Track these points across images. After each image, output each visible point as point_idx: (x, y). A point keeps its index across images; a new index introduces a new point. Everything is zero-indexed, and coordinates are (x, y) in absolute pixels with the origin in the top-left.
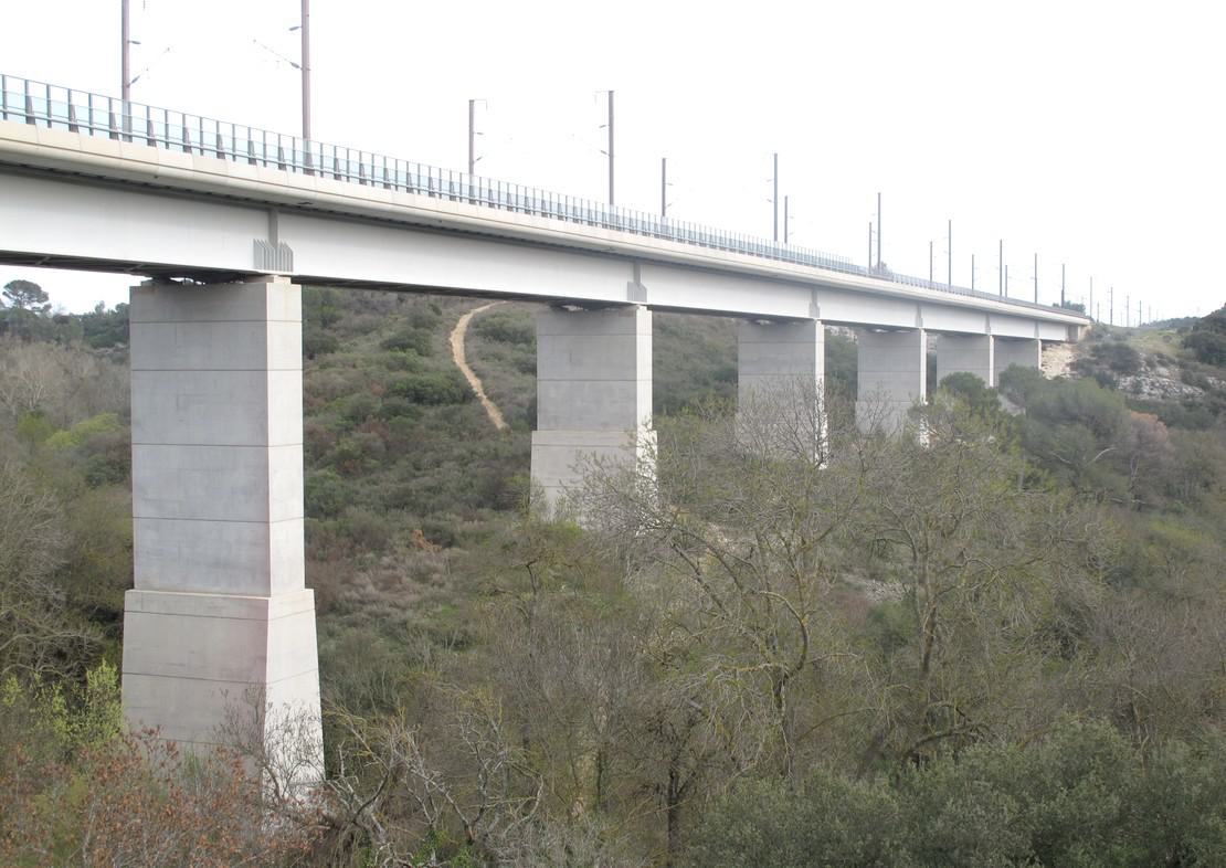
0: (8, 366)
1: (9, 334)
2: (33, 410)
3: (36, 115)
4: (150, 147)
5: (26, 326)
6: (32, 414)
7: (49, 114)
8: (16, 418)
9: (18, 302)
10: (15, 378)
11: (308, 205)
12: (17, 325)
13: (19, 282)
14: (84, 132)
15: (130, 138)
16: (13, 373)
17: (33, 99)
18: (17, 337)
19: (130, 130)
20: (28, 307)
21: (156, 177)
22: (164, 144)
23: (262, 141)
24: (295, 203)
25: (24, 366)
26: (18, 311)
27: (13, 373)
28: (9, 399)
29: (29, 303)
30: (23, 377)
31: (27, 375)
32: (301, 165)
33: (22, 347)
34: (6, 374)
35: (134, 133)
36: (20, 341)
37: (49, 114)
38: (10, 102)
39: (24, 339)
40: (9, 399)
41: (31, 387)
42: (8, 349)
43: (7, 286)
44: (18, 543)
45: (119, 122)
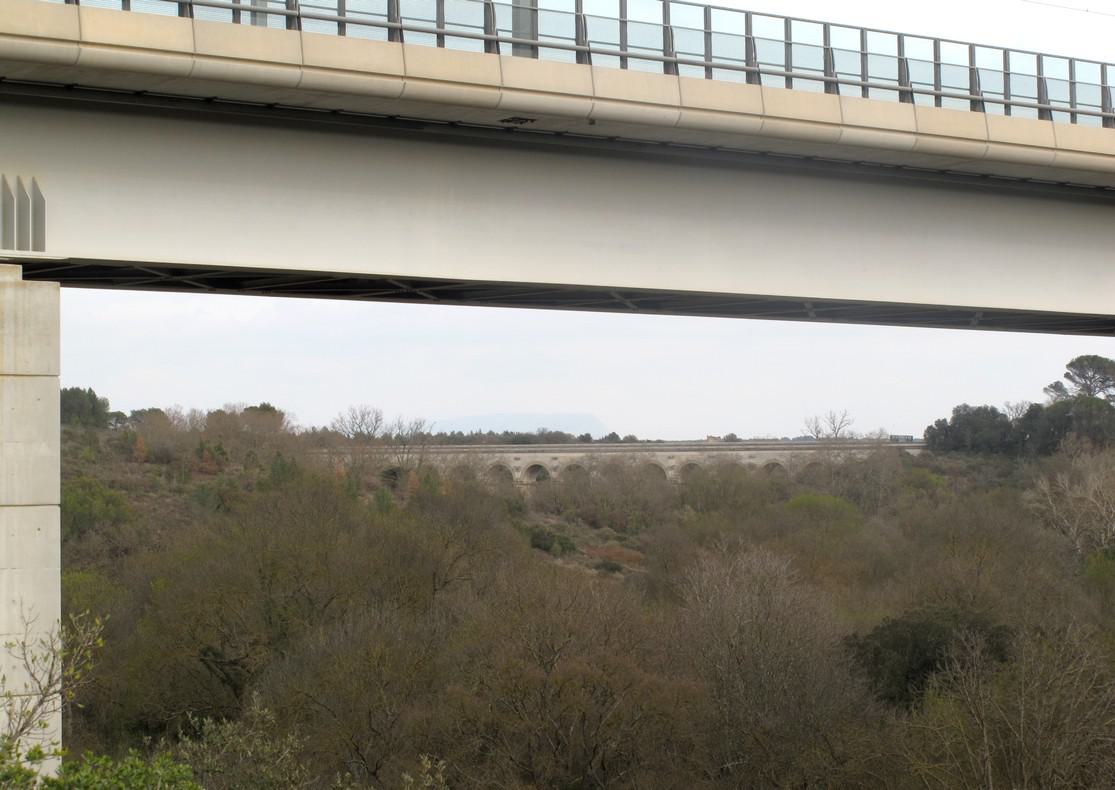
0: (1072, 483)
1: (1074, 434)
2: (1106, 547)
3: (1053, 104)
4: (623, 70)
5: (1097, 423)
6: (1106, 552)
7: (1073, 102)
8: (1082, 558)
9: (1086, 388)
10: (1082, 500)
11: (527, 126)
12: (1084, 422)
13: (1087, 358)
14: (994, 110)
15: (533, 50)
16: (1078, 492)
17: (675, 31)
18: (1085, 439)
19: (534, 34)
20: (1101, 396)
21: (592, 122)
22: (334, 26)
23: (660, 21)
24: (493, 120)
25: (1094, 481)
26: (1086, 401)
27: (1078, 492)
28: (1073, 531)
29: (1102, 389)
30: (1092, 499)
31: (1098, 494)
32: (509, 36)
33: (1092, 454)
34: (1069, 494)
35: (541, 40)
36: (1088, 446)
37: (1073, 102)
38: (679, 44)
39: (1094, 441)
40: (1073, 531)
41: (1104, 513)
42: (1071, 456)
43: (1071, 365)
44: (1084, 744)
45: (504, 22)
